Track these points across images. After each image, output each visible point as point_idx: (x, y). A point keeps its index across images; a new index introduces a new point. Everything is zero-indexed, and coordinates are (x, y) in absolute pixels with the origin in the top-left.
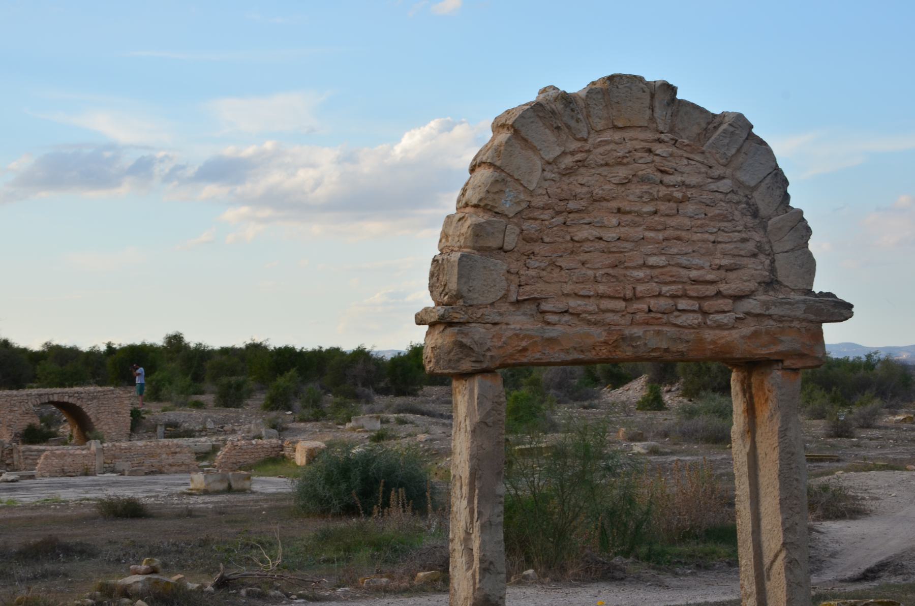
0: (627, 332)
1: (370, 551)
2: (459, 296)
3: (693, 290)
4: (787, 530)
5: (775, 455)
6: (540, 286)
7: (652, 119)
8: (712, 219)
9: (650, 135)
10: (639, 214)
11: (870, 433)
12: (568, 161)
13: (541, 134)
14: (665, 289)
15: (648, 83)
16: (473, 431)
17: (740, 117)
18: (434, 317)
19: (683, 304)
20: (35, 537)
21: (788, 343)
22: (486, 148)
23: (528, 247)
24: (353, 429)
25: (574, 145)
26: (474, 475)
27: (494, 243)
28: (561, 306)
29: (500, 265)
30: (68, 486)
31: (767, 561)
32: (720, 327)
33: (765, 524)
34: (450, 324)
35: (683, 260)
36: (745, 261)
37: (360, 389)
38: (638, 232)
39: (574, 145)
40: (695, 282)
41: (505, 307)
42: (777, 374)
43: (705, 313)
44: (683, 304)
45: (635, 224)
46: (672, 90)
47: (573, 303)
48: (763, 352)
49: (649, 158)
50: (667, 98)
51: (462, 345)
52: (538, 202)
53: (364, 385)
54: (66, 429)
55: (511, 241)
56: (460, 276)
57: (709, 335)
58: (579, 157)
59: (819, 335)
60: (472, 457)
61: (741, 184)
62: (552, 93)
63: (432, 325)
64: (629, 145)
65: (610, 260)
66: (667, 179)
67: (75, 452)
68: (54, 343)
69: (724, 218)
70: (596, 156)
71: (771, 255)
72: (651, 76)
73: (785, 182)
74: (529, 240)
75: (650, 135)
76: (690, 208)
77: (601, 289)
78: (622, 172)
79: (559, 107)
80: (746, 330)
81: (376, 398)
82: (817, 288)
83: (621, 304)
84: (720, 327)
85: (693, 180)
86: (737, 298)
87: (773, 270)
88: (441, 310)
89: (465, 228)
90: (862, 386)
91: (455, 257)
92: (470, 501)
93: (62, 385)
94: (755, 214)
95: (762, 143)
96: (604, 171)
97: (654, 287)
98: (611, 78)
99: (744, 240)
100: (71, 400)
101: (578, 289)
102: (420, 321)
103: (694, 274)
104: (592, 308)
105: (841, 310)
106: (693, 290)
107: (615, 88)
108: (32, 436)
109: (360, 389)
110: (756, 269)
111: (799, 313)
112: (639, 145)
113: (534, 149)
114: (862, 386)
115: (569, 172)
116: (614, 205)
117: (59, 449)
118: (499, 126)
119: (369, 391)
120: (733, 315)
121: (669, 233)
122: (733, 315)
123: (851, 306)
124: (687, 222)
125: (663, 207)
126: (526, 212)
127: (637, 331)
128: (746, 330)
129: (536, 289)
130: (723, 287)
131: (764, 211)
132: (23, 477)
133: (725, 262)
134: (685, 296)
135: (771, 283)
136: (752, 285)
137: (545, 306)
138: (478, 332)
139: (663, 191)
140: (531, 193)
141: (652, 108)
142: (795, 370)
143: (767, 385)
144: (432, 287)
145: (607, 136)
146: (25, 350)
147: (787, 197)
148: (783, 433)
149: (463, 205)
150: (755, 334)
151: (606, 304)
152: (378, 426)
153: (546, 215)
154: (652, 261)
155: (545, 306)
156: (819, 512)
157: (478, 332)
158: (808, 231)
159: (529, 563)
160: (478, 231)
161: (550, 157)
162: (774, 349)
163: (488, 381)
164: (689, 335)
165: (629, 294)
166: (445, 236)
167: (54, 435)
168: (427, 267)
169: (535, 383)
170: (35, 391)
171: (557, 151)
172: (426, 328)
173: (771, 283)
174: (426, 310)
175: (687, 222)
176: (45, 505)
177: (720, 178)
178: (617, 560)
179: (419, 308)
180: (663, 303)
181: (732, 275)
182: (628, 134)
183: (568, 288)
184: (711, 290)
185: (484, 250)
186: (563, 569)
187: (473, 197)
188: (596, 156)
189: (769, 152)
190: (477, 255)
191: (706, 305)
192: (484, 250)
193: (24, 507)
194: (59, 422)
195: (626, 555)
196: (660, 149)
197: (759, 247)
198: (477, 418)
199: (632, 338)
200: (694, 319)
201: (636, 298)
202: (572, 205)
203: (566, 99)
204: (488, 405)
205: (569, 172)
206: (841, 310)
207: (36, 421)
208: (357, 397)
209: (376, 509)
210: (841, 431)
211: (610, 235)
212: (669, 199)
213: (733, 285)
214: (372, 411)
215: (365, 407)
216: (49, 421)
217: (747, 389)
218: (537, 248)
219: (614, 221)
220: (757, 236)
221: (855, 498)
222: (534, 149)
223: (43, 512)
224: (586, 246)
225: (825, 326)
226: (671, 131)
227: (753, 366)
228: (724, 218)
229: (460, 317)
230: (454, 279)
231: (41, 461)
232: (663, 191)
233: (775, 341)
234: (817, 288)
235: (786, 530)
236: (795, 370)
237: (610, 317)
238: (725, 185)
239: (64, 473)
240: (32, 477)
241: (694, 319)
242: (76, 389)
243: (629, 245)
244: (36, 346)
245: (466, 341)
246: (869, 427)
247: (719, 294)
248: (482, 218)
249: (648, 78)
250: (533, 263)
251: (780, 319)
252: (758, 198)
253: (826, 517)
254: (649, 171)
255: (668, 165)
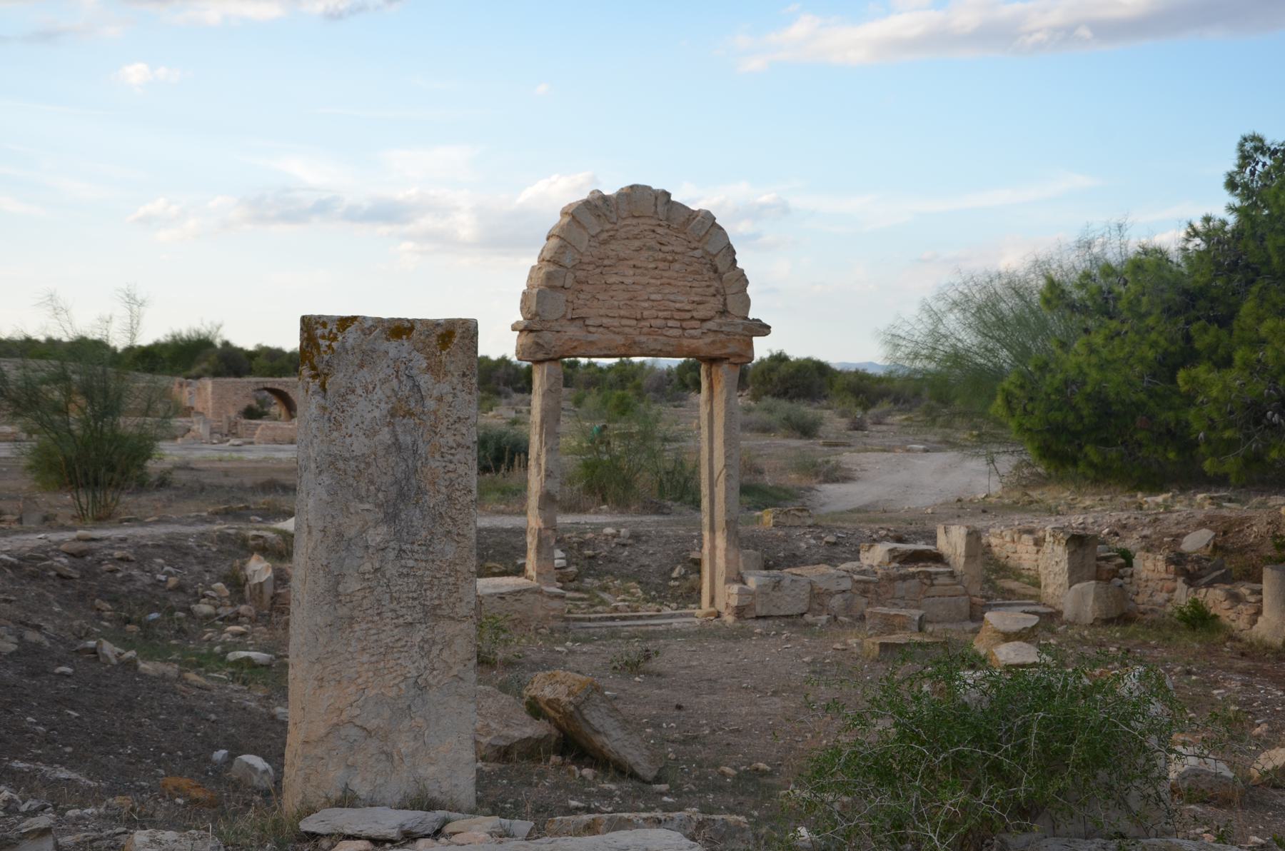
0: (637, 339)
1: (498, 495)
2: (537, 314)
3: (677, 315)
4: (727, 457)
5: (723, 414)
6: (586, 310)
7: (656, 212)
8: (691, 272)
9: (654, 222)
10: (646, 269)
11: (879, 428)
12: (605, 236)
13: (588, 219)
14: (660, 314)
15: (654, 191)
16: (543, 395)
17: (708, 213)
18: (522, 327)
19: (670, 323)
20: (261, 478)
21: (732, 348)
22: (556, 226)
23: (579, 287)
24: (494, 417)
25: (608, 226)
26: (542, 421)
27: (559, 283)
28: (598, 322)
29: (562, 297)
30: (280, 451)
31: (716, 476)
32: (692, 337)
33: (716, 454)
34: (531, 331)
35: (672, 297)
36: (709, 299)
37: (502, 387)
38: (645, 280)
39: (608, 226)
40: (679, 310)
41: (564, 322)
42: (725, 366)
43: (684, 329)
44: (670, 323)
45: (644, 275)
46: (668, 195)
47: (605, 321)
48: (717, 353)
49: (653, 235)
50: (665, 199)
51: (537, 344)
52: (585, 260)
53: (505, 384)
54: (277, 409)
55: (568, 283)
56: (538, 303)
57: (685, 342)
58: (612, 233)
59: (750, 345)
60: (542, 410)
61: (708, 253)
62: (597, 195)
63: (521, 331)
64: (642, 227)
65: (627, 295)
66: (663, 248)
67: (284, 426)
68: (264, 344)
69: (696, 273)
70: (622, 233)
71: (724, 295)
72: (656, 186)
73: (734, 252)
74: (579, 282)
75: (654, 222)
76: (677, 266)
77: (622, 313)
78: (637, 243)
79: (600, 203)
80: (708, 339)
81: (514, 395)
82: (751, 316)
83: (634, 322)
84: (692, 337)
85: (679, 249)
86: (703, 320)
87: (725, 305)
88: (526, 322)
89: (542, 274)
90: (883, 395)
91: (535, 291)
92: (541, 436)
93: (271, 376)
94: (716, 271)
95: (721, 228)
96: (626, 242)
97: (654, 313)
98: (632, 187)
99: (708, 286)
100: (280, 388)
101: (608, 312)
102: (514, 329)
103: (678, 305)
104: (616, 324)
105: (764, 329)
106: (677, 315)
107: (635, 194)
108: (250, 413)
109: (502, 387)
110: (715, 303)
111: (740, 330)
112: (647, 227)
113: (584, 228)
114: (883, 395)
115: (605, 242)
116: (632, 263)
117: (271, 424)
118: (564, 213)
119: (509, 389)
120: (699, 331)
121: (664, 280)
122: (699, 331)
123: (769, 327)
124: (675, 275)
125: (661, 265)
126: (579, 265)
127: (643, 339)
128: (708, 339)
129: (582, 312)
130: (695, 314)
131: (721, 269)
132: (246, 443)
133: (696, 299)
134: (672, 318)
135: (724, 312)
136: (713, 313)
137: (588, 322)
138: (547, 336)
139: (661, 255)
140: (582, 254)
141: (656, 205)
142: (736, 364)
143: (720, 372)
144: (522, 309)
145: (628, 222)
146: (241, 350)
147: (735, 261)
148: (727, 401)
149: (541, 260)
150: (713, 342)
151: (625, 322)
152: (513, 415)
153: (591, 267)
154: (653, 297)
155: (588, 322)
156: (821, 478)
157: (547, 336)
158: (747, 282)
159: (604, 501)
160: (549, 276)
161: (593, 233)
162: (724, 351)
163: (553, 365)
164: (673, 341)
165: (639, 317)
166: (530, 278)
167: (266, 414)
168: (520, 297)
169: (638, 387)
170: (253, 379)
171: (598, 230)
172: (517, 333)
173: (724, 312)
174: (518, 322)
175: (675, 275)
176: (265, 460)
177: (695, 249)
178: (669, 503)
179: (513, 321)
180: (659, 322)
181: (701, 307)
182: (641, 221)
183: (602, 312)
184: (688, 315)
185: (553, 288)
186: (628, 506)
187: (547, 256)
188: (622, 233)
189: (725, 234)
190: (548, 290)
191: (684, 324)
192: (553, 288)
193: (250, 461)
194: (270, 404)
195: (675, 500)
196: (659, 230)
197: (718, 291)
198: (546, 387)
199: (640, 343)
200: (677, 332)
201: (643, 319)
202: (606, 262)
203: (605, 199)
204: (553, 380)
205: (605, 242)
206: (764, 329)
207: (254, 403)
208: (498, 393)
209: (503, 467)
210: (858, 426)
211: (628, 281)
212: (665, 260)
213: (702, 312)
214: (509, 404)
215: (504, 401)
216: (263, 403)
217: (709, 375)
218: (584, 287)
219: (631, 273)
220: (716, 284)
221: (850, 470)
222: (584, 228)
223: (264, 464)
224: (614, 287)
225: (755, 339)
226: (667, 219)
227: (713, 361)
228: (696, 273)
229: (537, 327)
230: (534, 304)
231: (258, 432)
232: (661, 255)
233: (725, 347)
234: (751, 316)
235: (727, 457)
236: (736, 364)
237: (627, 330)
238: (698, 253)
239: (275, 441)
240: (252, 443)
241: (677, 332)
242: (285, 379)
243: (639, 287)
244: (250, 346)
245: (541, 341)
246: (880, 423)
247: (692, 318)
248: (552, 268)
249: (654, 187)
250: (581, 296)
251: (728, 334)
252: (717, 261)
253: (826, 482)
254: (653, 243)
255: (664, 240)
